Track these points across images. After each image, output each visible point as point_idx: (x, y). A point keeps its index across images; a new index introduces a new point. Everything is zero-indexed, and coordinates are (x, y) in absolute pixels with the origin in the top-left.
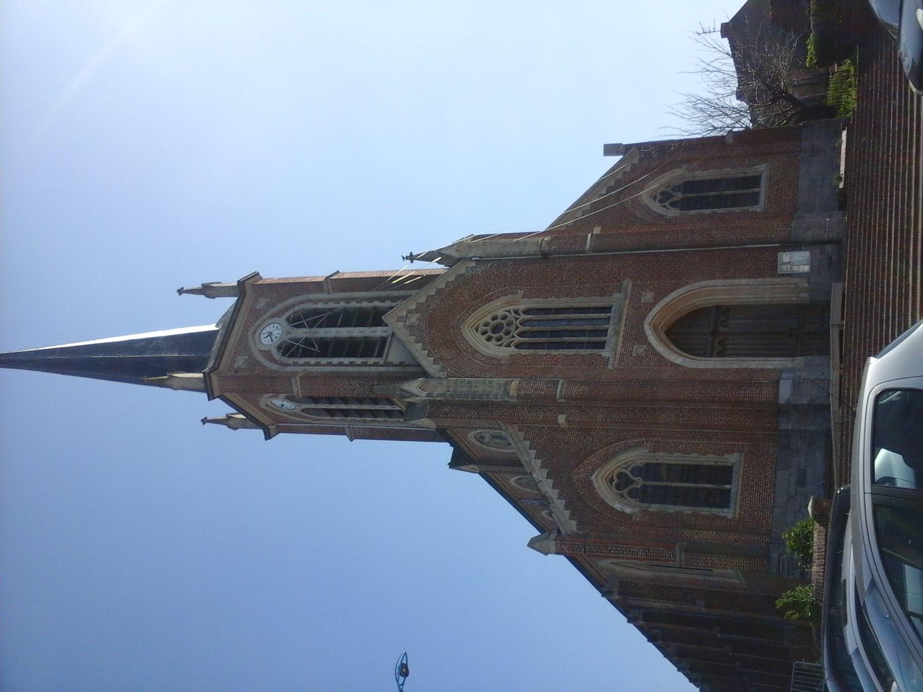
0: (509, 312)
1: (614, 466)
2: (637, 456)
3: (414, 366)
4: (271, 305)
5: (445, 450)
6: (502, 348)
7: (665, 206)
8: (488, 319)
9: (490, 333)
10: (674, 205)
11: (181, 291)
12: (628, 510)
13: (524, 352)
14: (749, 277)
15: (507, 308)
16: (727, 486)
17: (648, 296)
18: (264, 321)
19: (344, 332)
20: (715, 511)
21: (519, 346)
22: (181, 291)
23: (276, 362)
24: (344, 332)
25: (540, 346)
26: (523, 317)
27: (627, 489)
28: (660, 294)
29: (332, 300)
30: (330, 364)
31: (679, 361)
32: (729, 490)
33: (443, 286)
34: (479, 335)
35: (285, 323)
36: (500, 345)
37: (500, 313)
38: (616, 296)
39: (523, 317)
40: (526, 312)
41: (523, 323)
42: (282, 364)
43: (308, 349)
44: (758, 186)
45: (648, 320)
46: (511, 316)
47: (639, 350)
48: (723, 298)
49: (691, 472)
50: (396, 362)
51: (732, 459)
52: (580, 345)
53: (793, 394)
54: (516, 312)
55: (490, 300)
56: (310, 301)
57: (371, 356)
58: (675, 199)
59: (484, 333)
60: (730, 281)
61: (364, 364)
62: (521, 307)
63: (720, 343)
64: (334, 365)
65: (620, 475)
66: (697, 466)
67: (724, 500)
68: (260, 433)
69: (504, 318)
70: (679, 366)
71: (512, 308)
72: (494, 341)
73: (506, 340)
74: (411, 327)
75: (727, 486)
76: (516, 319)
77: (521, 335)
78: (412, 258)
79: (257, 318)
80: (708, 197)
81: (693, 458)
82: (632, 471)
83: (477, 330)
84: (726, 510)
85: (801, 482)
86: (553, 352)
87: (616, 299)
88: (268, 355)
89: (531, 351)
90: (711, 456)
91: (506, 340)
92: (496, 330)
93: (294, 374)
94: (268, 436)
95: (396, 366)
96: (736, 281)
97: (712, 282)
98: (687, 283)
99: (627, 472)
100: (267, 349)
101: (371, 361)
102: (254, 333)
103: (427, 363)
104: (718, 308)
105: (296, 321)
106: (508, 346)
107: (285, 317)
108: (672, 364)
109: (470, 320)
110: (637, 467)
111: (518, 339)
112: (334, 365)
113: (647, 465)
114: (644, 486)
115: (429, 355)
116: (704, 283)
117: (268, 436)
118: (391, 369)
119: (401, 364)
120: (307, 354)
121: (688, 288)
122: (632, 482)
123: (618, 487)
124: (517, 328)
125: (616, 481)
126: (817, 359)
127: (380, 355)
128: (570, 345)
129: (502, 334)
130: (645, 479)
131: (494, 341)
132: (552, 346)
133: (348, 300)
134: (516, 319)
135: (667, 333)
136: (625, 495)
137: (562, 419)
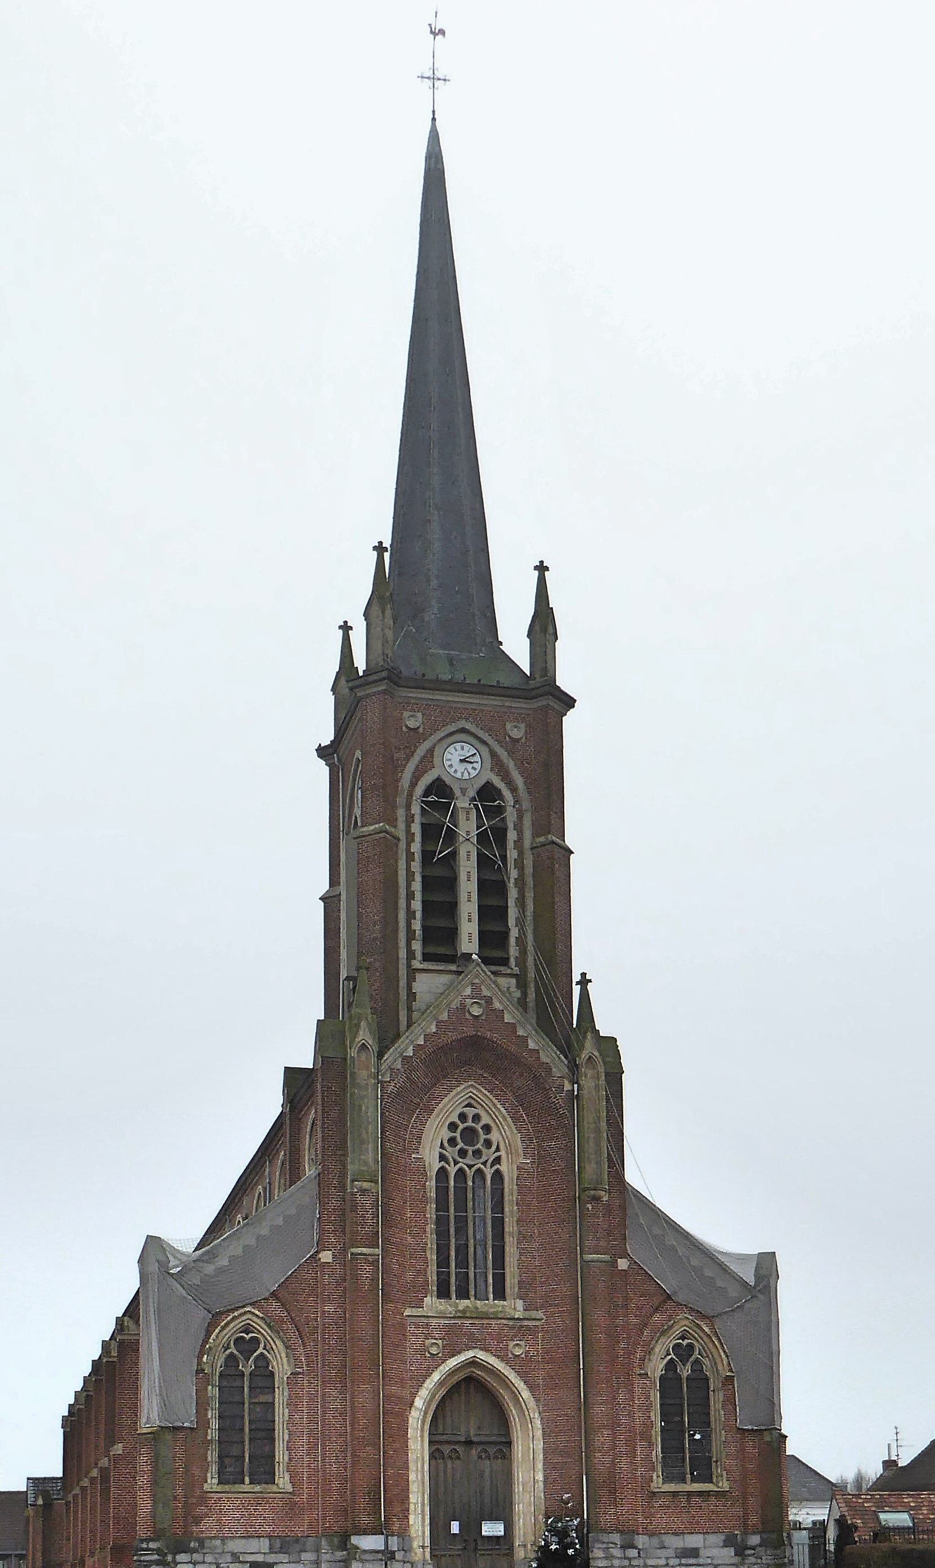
0: (498, 1149)
2: (281, 1366)
3: (409, 1018)
5: (306, 1060)
6: (438, 1150)
8: (485, 1120)
9: (470, 1123)
10: (671, 1366)
11: (541, 568)
13: (432, 1184)
14: (545, 1482)
15: (502, 1146)
16: (247, 1480)
19: (468, 887)
20: (214, 1468)
21: (442, 1173)
22: (541, 568)
24: (468, 887)
25: (442, 1203)
26: (489, 1172)
27: (235, 1352)
28: (523, 1367)
29: (521, 853)
30: (410, 876)
31: (419, 1403)
33: (532, 1045)
34: (459, 1110)
35: (482, 782)
36: (442, 1146)
37: (494, 1136)
38: (520, 1304)
39: (489, 1172)
40: (498, 1176)
43: (437, 834)
45: (481, 1355)
46: (489, 1155)
48: (519, 1449)
49: (265, 1433)
51: (283, 1481)
52: (443, 1262)
54: (498, 1160)
55: (516, 1119)
56: (520, 817)
57: (426, 941)
59: (463, 1117)
60: (541, 1457)
61: (411, 935)
62: (504, 1168)
66: (273, 1440)
68: (327, 737)
69: (488, 1143)
70: (412, 1404)
71: (502, 1153)
73: (451, 1153)
74: (463, 1008)
75: (247, 1480)
76: (484, 1163)
77: (461, 1173)
78: (584, 981)
80: (682, 1414)
84: (215, 1481)
86: (431, 1227)
87: (514, 1307)
88: (428, 761)
90: (286, 1458)
91: (451, 1153)
92: (468, 1134)
93: (393, 822)
94: (323, 752)
95: (409, 987)
96: (540, 1466)
97: (539, 1433)
98: (537, 1401)
99: (696, 1354)
100: (436, 761)
101: (417, 946)
102: (463, 730)
103: (406, 1046)
104: (509, 1444)
105: (487, 793)
106: (442, 1158)
108: (414, 1395)
109: (483, 1094)
111: (452, 1170)
113: (272, 1374)
115: (418, 1048)
116: (538, 1423)
117: (323, 752)
118: (403, 982)
119: (412, 996)
120: (430, 832)
121: (532, 1403)
123: (239, 1341)
124: (470, 1167)
127: (427, 957)
128: (442, 1251)
129: (461, 1145)
132: (441, 1222)
134: (484, 1163)
135: (469, 1380)
136: (228, 1351)
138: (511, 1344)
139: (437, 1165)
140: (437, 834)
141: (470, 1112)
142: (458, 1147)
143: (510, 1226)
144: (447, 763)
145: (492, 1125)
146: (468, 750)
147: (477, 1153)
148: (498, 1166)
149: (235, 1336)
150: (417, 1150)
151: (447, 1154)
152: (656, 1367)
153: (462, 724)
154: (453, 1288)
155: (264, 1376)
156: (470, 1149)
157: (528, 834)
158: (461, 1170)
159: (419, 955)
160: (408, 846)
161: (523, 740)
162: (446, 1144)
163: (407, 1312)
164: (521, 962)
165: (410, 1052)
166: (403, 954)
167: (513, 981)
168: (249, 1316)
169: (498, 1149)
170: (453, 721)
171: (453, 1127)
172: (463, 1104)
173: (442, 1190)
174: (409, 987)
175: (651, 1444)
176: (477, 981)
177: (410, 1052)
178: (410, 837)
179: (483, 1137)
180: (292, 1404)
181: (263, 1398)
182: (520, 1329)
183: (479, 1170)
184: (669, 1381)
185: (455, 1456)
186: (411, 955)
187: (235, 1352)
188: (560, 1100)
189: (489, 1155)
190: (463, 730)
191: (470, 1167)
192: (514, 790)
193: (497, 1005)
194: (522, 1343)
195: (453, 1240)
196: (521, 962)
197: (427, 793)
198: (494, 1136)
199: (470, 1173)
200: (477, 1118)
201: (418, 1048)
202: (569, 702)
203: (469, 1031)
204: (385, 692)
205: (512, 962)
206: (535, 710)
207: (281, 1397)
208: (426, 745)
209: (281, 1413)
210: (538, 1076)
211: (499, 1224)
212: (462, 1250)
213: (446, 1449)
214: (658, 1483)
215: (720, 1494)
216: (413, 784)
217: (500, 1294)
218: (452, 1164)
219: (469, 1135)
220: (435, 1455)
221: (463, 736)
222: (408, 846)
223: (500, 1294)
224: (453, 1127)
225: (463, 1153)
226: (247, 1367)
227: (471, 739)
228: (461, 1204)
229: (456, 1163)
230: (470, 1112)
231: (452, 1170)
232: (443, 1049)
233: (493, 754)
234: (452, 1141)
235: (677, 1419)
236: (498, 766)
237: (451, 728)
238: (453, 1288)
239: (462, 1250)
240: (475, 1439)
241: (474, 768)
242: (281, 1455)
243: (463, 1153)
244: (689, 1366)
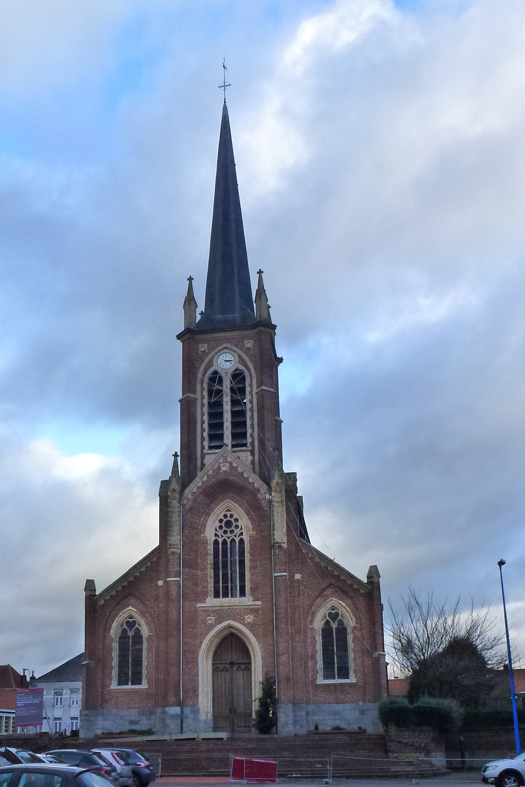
0: (241, 529)
1: (138, 618)
2: (145, 631)
4: (247, 351)
7: (342, 616)
9: (229, 519)
11: (190, 279)
12: (112, 632)
16: (130, 683)
17: (249, 618)
18: (235, 352)
21: (216, 542)
22: (190, 279)
23: (204, 375)
27: (126, 627)
28: (251, 627)
32: (128, 685)
34: (224, 513)
35: (234, 368)
36: (216, 530)
37: (239, 524)
39: (237, 540)
40: (242, 541)
41: (233, 541)
42: (202, 381)
43: (215, 394)
44: (340, 677)
46: (237, 531)
47: (211, 620)
49: (138, 662)
50: (205, 461)
52: (216, 582)
53: (172, 715)
54: (241, 534)
58: (332, 623)
59: (225, 516)
62: (244, 537)
63: (225, 667)
64: (202, 418)
65: (337, 614)
67: (122, 681)
69: (237, 527)
71: (243, 530)
72: (238, 524)
73: (220, 532)
75: (130, 683)
77: (225, 542)
79: (236, 346)
81: (145, 663)
82: (340, 620)
83: (227, 511)
85: (132, 722)
88: (210, 364)
89: (212, 552)
91: (220, 532)
92: (228, 524)
98: (259, 643)
99: (340, 617)
102: (226, 348)
105: (238, 377)
106: (216, 535)
107: (241, 367)
110: (140, 631)
111: (220, 540)
112: (202, 418)
114: (129, 637)
122: (131, 630)
123: (330, 614)
125: (333, 612)
126: (211, 725)
128: (216, 576)
130: (133, 637)
131: (238, 524)
133: (251, 410)
134: (235, 536)
137: (298, 576)
138: (246, 617)
139: (214, 538)
140: (215, 394)
141: (228, 513)
142: (223, 529)
143: (247, 564)
144: (219, 363)
145: (239, 518)
146: (229, 357)
147: (232, 532)
148: (241, 536)
149: (126, 620)
150: (204, 533)
151: (218, 534)
152: (318, 624)
153: (225, 345)
154: (221, 593)
155: (138, 637)
156: (229, 530)
157: (255, 387)
158: (225, 539)
159: (206, 447)
160: (202, 401)
161: (252, 347)
162: (218, 529)
163: (199, 605)
164: (252, 444)
165: (195, 490)
166: (199, 448)
167: (249, 453)
168: (130, 611)
169: (241, 529)
170: (221, 345)
171: (221, 521)
172: (225, 510)
173: (216, 550)
174: (202, 462)
175: (316, 662)
176: (225, 455)
177: (195, 490)
178: (203, 397)
179: (234, 524)
180: (149, 650)
181: (137, 647)
182: (253, 611)
183: (233, 539)
184: (327, 632)
185: (225, 670)
186: (203, 448)
187: (126, 627)
188: (264, 503)
189: (237, 531)
190: (226, 348)
191: (229, 538)
192: (249, 370)
193: (234, 465)
194: (252, 616)
195: (221, 572)
196: (252, 444)
197: (244, 377)
198: (239, 524)
199: (229, 541)
200: (231, 516)
201: (199, 488)
202: (275, 327)
203: (221, 477)
204: (189, 338)
205: (249, 445)
206: (257, 333)
207: (145, 645)
208: (210, 356)
209: (145, 653)
210: (254, 493)
211: (242, 562)
212: (225, 575)
213: (221, 667)
214: (321, 681)
215: (351, 685)
216: (204, 375)
217: (243, 593)
218: (220, 537)
219: (229, 524)
220: (216, 669)
221: (226, 351)
222: (202, 401)
223: (243, 593)
224: (221, 521)
225: (225, 532)
226: (131, 634)
227: (230, 351)
228: (225, 555)
229: (222, 537)
230: (228, 513)
231: (220, 540)
232: (212, 487)
233: (239, 356)
234: (221, 527)
235: (331, 648)
236: (242, 361)
237: (220, 348)
238: (221, 593)
239: (225, 575)
240: (235, 662)
241: (231, 363)
242: (145, 672)
243: (225, 532)
244: (336, 623)
